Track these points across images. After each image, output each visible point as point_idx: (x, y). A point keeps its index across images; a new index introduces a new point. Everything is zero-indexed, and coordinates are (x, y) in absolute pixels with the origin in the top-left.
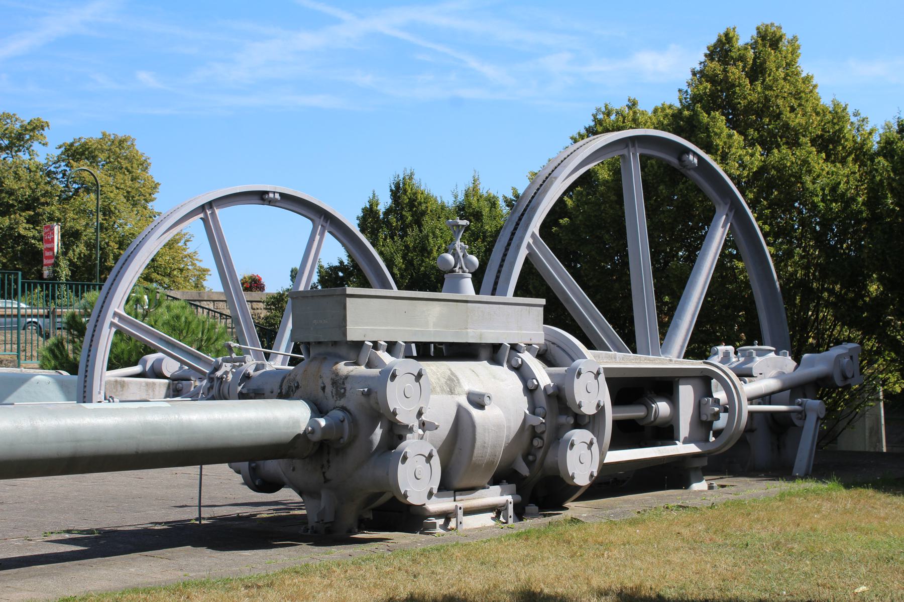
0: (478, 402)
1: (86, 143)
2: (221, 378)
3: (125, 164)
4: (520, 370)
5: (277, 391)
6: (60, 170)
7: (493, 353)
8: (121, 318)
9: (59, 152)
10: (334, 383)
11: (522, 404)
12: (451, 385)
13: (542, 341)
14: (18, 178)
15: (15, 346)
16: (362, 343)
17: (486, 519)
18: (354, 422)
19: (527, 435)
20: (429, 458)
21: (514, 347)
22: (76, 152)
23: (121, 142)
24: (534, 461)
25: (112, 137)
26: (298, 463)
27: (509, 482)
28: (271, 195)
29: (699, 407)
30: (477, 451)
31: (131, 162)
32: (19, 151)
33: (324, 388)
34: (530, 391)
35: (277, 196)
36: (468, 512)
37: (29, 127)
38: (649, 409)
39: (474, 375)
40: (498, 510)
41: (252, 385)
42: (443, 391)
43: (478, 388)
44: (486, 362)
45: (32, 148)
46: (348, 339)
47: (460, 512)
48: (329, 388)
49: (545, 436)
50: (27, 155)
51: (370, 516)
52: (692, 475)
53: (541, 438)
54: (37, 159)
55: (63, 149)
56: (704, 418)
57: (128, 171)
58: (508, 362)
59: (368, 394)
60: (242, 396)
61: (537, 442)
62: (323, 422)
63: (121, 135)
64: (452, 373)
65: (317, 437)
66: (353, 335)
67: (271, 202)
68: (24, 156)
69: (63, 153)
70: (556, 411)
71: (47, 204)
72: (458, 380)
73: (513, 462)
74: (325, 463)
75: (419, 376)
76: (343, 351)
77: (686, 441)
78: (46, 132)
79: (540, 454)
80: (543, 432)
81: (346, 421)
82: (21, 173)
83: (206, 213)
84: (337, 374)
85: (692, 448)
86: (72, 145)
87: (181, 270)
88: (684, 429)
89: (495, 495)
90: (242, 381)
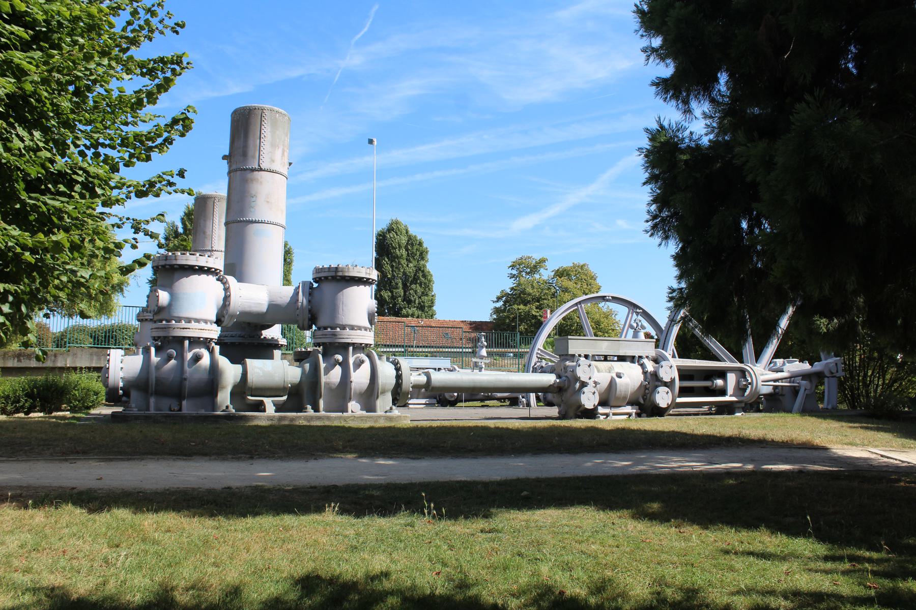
0: (619, 376)
4: (642, 366)
7: (632, 359)
11: (641, 377)
12: (610, 370)
14: (533, 287)
17: (625, 417)
18: (569, 381)
19: (643, 389)
20: (594, 393)
21: (640, 357)
22: (561, 273)
23: (582, 267)
29: (738, 382)
34: (645, 373)
36: (614, 414)
40: (630, 415)
66: (570, 352)
67: (608, 300)
68: (537, 276)
70: (653, 380)
75: (590, 366)
78: (547, 263)
85: (734, 399)
87: (613, 330)
88: (730, 390)
89: (628, 409)
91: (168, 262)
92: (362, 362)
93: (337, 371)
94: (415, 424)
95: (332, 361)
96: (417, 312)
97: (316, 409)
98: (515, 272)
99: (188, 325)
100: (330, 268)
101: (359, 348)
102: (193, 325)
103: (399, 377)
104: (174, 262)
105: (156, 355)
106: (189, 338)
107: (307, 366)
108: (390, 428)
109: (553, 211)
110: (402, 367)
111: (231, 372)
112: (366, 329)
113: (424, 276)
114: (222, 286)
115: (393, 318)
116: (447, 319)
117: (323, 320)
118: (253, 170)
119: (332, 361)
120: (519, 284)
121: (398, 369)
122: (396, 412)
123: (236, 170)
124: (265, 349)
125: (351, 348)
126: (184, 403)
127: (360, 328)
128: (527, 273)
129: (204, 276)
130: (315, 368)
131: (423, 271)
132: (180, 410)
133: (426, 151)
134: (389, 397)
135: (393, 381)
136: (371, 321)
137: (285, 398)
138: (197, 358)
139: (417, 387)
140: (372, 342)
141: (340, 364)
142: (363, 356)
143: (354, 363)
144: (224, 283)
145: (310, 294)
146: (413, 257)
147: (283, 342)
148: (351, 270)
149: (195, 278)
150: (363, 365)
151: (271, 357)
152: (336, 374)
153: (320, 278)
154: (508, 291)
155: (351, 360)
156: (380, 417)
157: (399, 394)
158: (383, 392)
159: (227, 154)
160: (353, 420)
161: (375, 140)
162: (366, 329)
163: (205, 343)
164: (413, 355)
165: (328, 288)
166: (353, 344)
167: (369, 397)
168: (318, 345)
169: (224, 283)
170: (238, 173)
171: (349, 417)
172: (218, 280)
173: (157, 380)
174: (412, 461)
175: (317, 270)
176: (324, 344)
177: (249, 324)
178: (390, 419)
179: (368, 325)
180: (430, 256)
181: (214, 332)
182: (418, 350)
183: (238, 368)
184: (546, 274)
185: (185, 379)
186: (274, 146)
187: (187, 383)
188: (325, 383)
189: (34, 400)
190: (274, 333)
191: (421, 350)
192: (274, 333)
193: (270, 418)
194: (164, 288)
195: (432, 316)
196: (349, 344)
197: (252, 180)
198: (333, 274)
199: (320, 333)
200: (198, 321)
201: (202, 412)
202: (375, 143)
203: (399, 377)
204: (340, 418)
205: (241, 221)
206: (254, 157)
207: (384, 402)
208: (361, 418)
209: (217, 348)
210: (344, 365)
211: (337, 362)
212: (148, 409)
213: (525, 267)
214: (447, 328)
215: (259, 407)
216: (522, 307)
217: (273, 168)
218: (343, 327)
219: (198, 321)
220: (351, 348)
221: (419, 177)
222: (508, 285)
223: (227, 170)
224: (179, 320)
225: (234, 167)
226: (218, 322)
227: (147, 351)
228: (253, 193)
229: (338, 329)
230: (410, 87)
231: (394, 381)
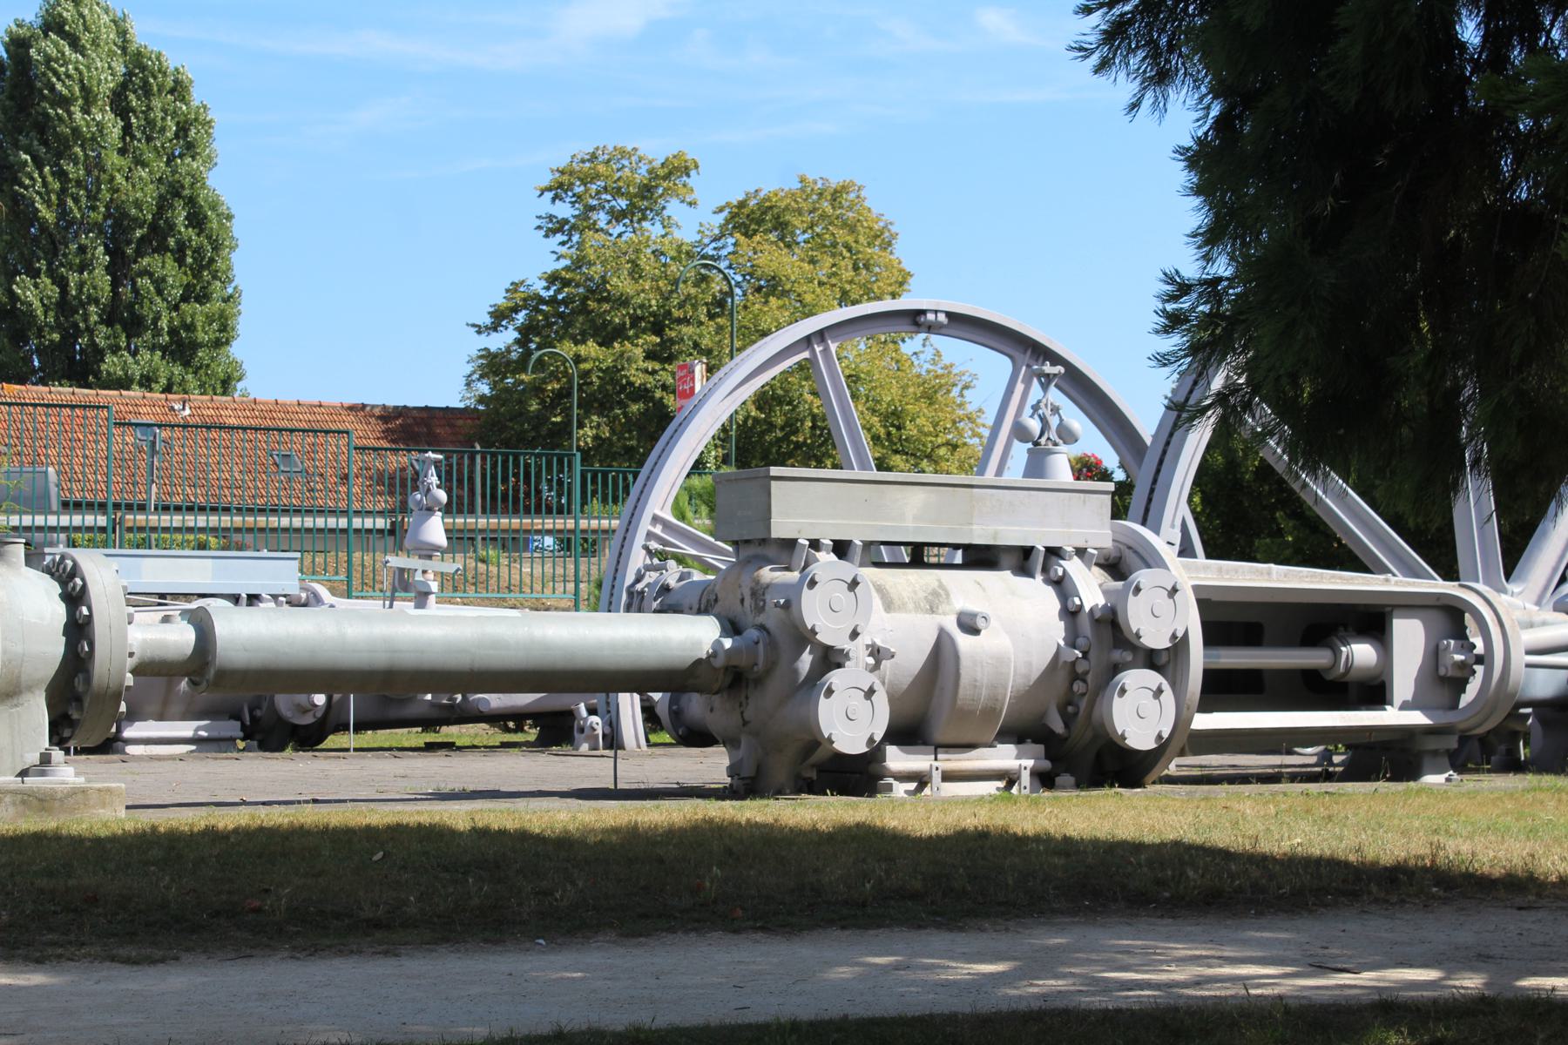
0: (969, 625)
1: (769, 199)
2: (642, 592)
3: (842, 235)
4: (1061, 585)
5: (696, 607)
6: (724, 252)
7: (1022, 560)
8: (666, 525)
9: (720, 218)
10: (754, 594)
11: (1057, 632)
13: (1108, 544)
14: (636, 272)
15: (571, 586)
16: (795, 541)
17: (990, 788)
18: (772, 645)
19: (1062, 677)
20: (870, 693)
21: (1054, 553)
22: (749, 219)
23: (836, 195)
24: (1076, 714)
25: (819, 185)
26: (717, 699)
27: (1035, 742)
28: (931, 317)
29: (1434, 654)
30: (964, 691)
31: (852, 229)
32: (644, 218)
33: (742, 601)
34: (1070, 614)
35: (942, 318)
36: (948, 777)
37: (661, 172)
38: (1337, 654)
39: (971, 589)
40: (1010, 779)
41: (671, 599)
42: (917, 608)
43: (971, 607)
44: (1008, 573)
45: (665, 213)
46: (774, 535)
47: (937, 776)
48: (748, 601)
49: (1089, 678)
50: (658, 225)
51: (813, 775)
52: (1427, 762)
53: (1085, 681)
54: (678, 235)
55: (725, 214)
56: (1442, 672)
57: (850, 250)
58: (1045, 570)
59: (787, 606)
60: (660, 610)
61: (1078, 687)
62: (728, 643)
63: (835, 181)
64: (941, 586)
65: (719, 662)
66: (777, 533)
67: (931, 328)
68: (654, 230)
69: (727, 221)
70: (1104, 643)
71: (685, 321)
72: (948, 595)
73: (1044, 715)
74: (743, 699)
75: (854, 584)
76: (771, 552)
77: (1405, 706)
78: (693, 180)
79: (1083, 704)
80: (1087, 673)
81: (761, 645)
82: (642, 262)
83: (813, 351)
84: (757, 582)
85: (1417, 718)
86: (742, 205)
88: (1404, 683)
89: (1005, 757)
90: (659, 594)
94: (145, 820)
96: (167, 369)
98: (564, 210)
103: (78, 630)
108: (38, 838)
110: (94, 591)
113: (197, 220)
115: (63, 392)
116: (288, 396)
120: (579, 263)
121: (74, 598)
122: (68, 773)
128: (617, 216)
131: (191, 201)
139: (153, 669)
154: (539, 287)
157: (78, 699)
164: (145, 539)
174: (126, 970)
178: (43, 802)
182: (165, 520)
184: (690, 221)
191: (177, 520)
195: (226, 385)
203: (78, 630)
213: (606, 191)
214: (275, 426)
216: (591, 348)
222: (536, 262)
231: (56, 648)
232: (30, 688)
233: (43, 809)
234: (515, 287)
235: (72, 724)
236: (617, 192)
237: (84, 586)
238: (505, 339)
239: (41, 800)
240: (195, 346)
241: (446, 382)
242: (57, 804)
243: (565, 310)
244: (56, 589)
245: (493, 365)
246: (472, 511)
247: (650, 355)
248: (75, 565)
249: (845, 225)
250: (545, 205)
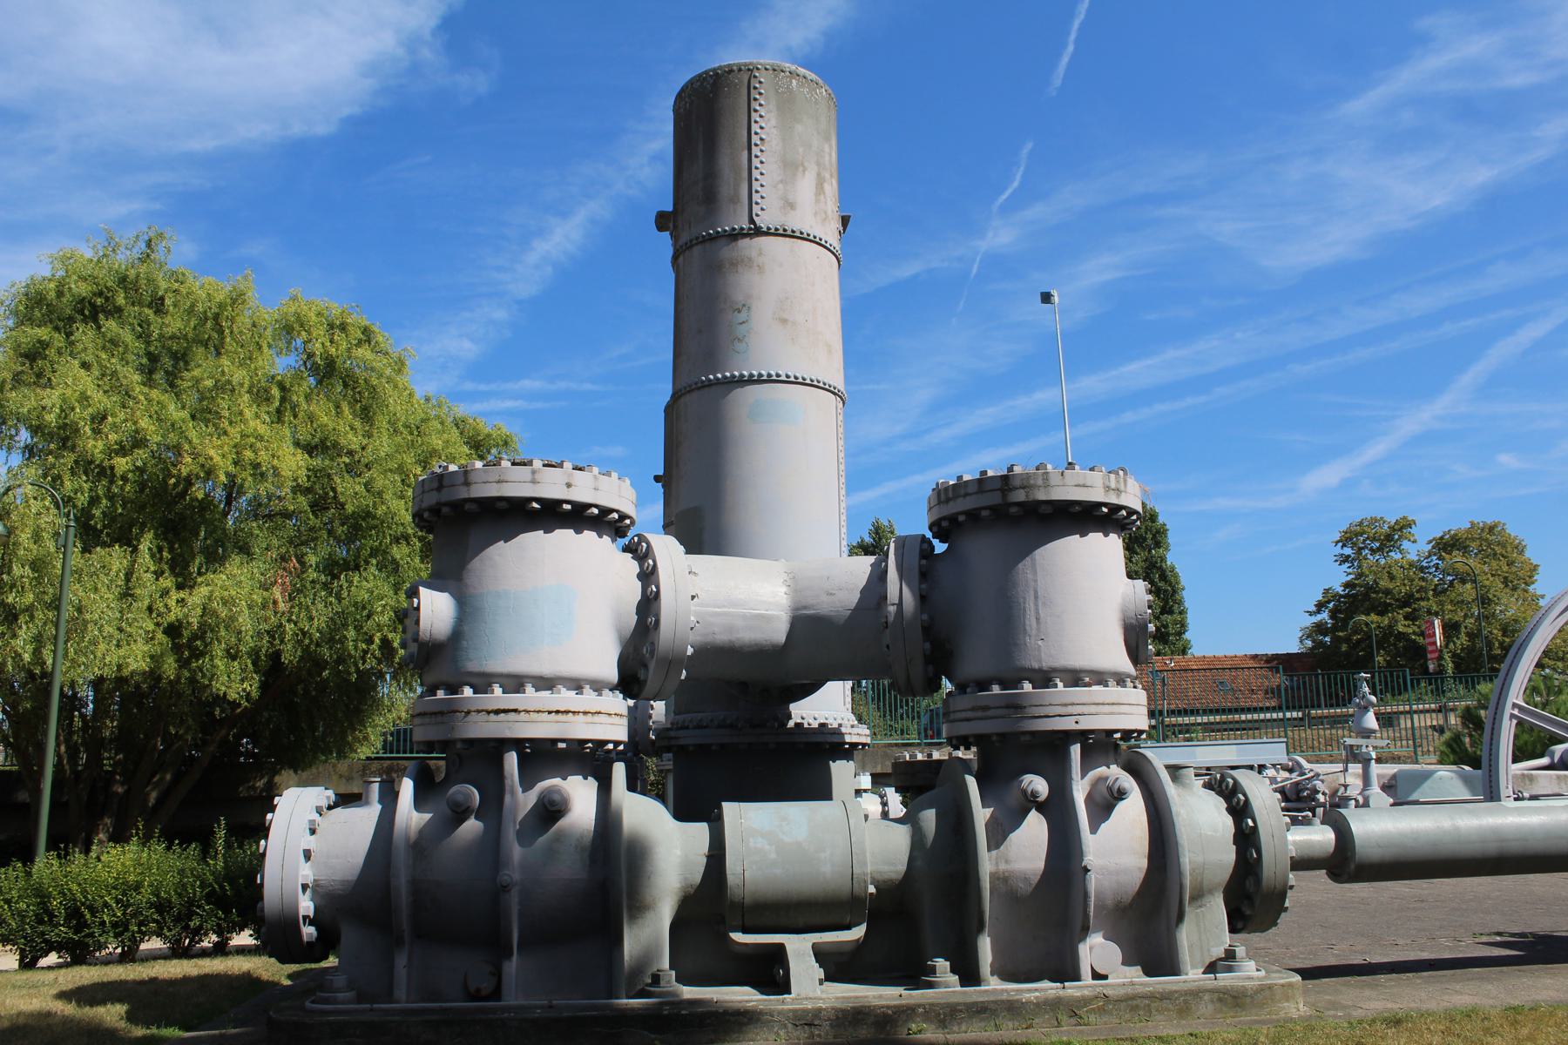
8: (1521, 708)
14: (1392, 578)
22: (1447, 545)
23: (1491, 529)
31: (1504, 546)
68: (1395, 556)
71: (1422, 599)
78: (1414, 530)
91: (445, 496)
92: (1121, 795)
93: (1033, 833)
95: (1013, 798)
97: (969, 975)
98: (1348, 551)
99: (513, 700)
100: (982, 482)
101: (1101, 745)
102: (531, 697)
103: (1246, 838)
104: (463, 493)
105: (419, 802)
106: (518, 744)
107: (929, 817)
109: (1376, 450)
111: (672, 847)
112: (1121, 680)
114: (634, 567)
116: (1219, 654)
117: (975, 662)
118: (735, 236)
119: (1013, 798)
120: (1360, 575)
123: (689, 246)
124: (800, 768)
125: (1076, 750)
126: (512, 967)
127: (1100, 678)
128: (1373, 551)
129: (564, 535)
130: (957, 823)
132: (496, 994)
133: (1137, 372)
134: (1216, 909)
135: (1227, 855)
136: (1135, 653)
137: (858, 932)
138: (551, 810)
140: (1141, 721)
141: (1042, 808)
142: (1115, 773)
143: (1089, 799)
144: (639, 551)
145: (924, 575)
146: (1141, 546)
147: (857, 733)
148: (1055, 479)
149: (533, 541)
150: (1121, 807)
151: (821, 791)
152: (1030, 841)
153: (953, 519)
154: (1340, 590)
155: (1080, 792)
156: (1196, 994)
158: (1199, 895)
159: (669, 208)
160: (1101, 1011)
161: (1055, 293)
162: (1121, 680)
163: (591, 759)
165: (981, 549)
166: (1082, 736)
167: (1149, 922)
168: (964, 742)
169: (639, 551)
170: (697, 250)
171: (1085, 1001)
172: (626, 549)
173: (419, 890)
175: (943, 495)
176: (980, 740)
177: (744, 686)
179: (1126, 666)
180: (1172, 538)
181: (606, 720)
183: (700, 831)
184: (1415, 548)
185: (505, 888)
186: (791, 167)
187: (514, 901)
188: (994, 877)
189: (227, 912)
190: (829, 706)
192: (829, 706)
193: (806, 1020)
194: (437, 581)
195: (1184, 652)
196: (1068, 737)
197: (735, 264)
198: (994, 499)
199: (964, 702)
200: (546, 683)
201: (573, 1002)
202: (1056, 299)
203: (1246, 838)
204: (1054, 1005)
205: (710, 384)
206: (735, 200)
207: (1204, 930)
208: (1133, 1003)
209: (619, 771)
210: (1057, 810)
211: (1030, 802)
212: (389, 996)
213: (1369, 540)
214: (1216, 668)
215: (769, 971)
216: (1374, 617)
217: (795, 222)
218: (1044, 679)
219: (546, 683)
220: (1076, 750)
221: (1128, 417)
222: (1338, 578)
223: (670, 252)
224: (483, 683)
225: (685, 237)
226: (629, 683)
227: (390, 797)
228: (739, 297)
229: (1027, 687)
230: (1098, 270)
231: (1229, 855)
232: (1211, 892)
233: (1237, 1005)
234: (1326, 591)
235: (1244, 917)
236: (1374, 539)
237: (1247, 800)
238: (1324, 616)
239: (1234, 997)
240: (1168, 634)
241: (1291, 644)
242: (1248, 1000)
243: (1347, 606)
244: (1221, 804)
245: (1319, 628)
246: (1319, 707)
247: (1406, 618)
248: (1236, 782)
249: (1499, 544)
250: (1338, 550)
